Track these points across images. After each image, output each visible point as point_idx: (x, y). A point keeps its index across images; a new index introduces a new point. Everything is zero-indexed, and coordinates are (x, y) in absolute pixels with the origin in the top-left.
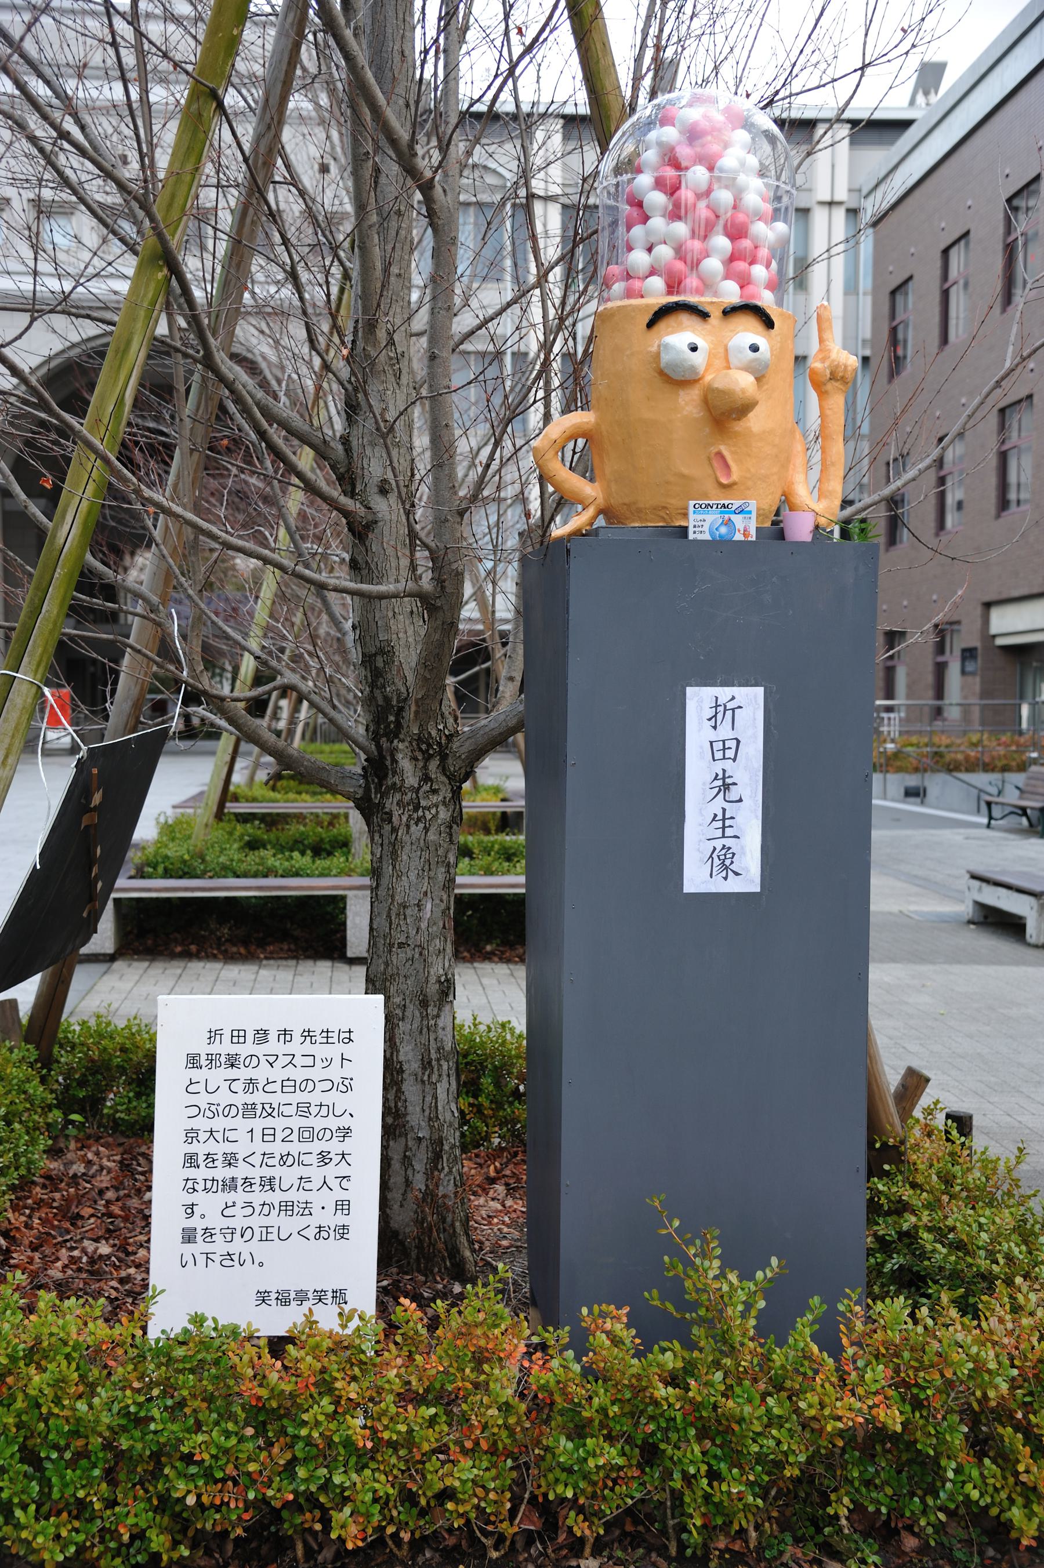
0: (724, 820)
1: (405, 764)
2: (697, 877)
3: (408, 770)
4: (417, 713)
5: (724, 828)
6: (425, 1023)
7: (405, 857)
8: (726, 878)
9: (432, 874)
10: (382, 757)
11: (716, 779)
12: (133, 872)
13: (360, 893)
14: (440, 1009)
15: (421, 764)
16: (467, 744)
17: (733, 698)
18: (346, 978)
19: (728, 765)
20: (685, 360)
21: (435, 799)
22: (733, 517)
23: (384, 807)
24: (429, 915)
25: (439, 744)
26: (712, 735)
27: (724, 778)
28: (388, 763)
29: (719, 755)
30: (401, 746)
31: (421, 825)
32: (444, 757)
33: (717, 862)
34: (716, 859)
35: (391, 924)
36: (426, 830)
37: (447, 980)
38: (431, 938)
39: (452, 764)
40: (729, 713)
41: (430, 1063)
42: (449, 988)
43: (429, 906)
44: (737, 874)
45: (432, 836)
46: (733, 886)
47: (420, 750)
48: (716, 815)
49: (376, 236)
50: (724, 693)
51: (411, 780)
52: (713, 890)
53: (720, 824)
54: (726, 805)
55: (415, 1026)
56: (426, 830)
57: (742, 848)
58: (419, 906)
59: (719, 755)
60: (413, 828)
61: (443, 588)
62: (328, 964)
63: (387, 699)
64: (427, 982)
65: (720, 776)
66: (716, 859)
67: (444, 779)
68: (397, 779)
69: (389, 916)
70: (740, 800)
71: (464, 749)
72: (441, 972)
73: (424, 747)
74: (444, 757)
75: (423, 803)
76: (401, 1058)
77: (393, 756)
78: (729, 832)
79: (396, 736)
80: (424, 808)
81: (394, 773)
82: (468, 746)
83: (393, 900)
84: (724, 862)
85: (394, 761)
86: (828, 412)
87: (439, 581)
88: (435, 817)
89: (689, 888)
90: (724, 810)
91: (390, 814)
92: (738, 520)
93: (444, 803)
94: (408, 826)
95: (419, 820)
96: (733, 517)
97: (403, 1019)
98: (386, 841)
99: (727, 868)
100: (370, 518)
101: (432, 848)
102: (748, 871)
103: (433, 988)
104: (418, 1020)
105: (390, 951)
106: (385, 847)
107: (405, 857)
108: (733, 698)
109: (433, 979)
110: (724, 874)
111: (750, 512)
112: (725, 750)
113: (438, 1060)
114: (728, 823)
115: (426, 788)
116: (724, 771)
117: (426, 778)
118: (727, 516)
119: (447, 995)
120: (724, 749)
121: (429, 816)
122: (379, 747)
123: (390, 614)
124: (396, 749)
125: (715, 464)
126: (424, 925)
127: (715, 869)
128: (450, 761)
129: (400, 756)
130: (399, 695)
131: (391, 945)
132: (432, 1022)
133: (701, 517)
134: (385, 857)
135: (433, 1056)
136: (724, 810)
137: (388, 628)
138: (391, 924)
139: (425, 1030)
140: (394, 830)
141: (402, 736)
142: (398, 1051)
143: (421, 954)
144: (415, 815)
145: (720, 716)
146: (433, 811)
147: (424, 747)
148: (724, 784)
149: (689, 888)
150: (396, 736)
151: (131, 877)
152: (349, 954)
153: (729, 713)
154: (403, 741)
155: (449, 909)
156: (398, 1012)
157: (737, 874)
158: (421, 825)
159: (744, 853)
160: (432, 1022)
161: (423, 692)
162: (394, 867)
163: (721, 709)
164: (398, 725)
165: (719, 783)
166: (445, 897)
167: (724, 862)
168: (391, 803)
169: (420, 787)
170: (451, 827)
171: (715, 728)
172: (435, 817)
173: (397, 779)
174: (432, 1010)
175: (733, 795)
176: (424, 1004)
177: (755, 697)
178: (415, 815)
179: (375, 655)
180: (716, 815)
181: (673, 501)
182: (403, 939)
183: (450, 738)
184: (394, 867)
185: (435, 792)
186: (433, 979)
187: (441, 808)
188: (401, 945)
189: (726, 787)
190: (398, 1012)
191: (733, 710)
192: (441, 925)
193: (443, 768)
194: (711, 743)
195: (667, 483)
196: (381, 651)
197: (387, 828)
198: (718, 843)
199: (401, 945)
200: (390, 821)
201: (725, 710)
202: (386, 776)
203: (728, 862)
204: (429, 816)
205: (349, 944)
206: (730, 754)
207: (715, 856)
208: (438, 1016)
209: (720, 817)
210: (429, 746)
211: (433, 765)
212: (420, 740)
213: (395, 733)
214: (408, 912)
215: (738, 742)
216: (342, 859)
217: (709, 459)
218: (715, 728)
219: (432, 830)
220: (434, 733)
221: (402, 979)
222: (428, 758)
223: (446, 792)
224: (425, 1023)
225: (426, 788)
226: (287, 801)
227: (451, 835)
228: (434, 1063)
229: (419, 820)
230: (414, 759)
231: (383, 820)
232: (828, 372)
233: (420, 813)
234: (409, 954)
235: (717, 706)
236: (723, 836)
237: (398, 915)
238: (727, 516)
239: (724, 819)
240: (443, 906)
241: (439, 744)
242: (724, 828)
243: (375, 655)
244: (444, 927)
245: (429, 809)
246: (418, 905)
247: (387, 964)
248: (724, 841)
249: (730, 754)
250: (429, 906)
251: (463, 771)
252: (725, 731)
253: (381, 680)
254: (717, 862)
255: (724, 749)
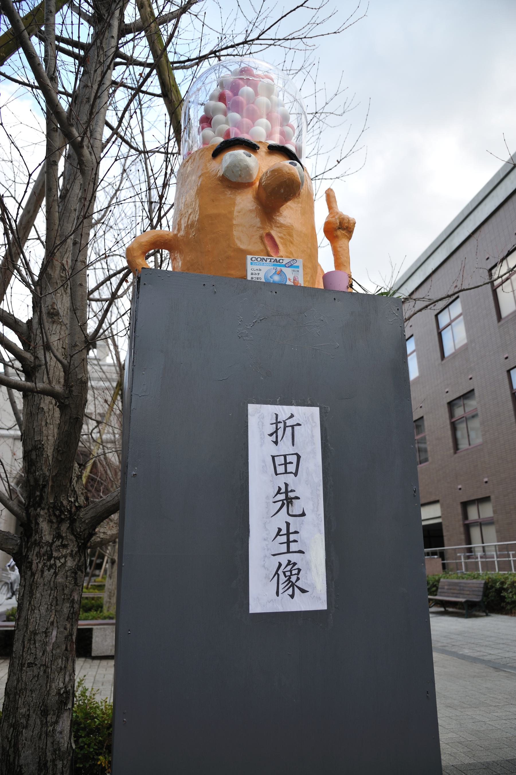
0: (288, 535)
1: (44, 526)
2: (263, 597)
3: (45, 530)
4: (52, 487)
5: (288, 542)
6: (44, 729)
7: (38, 595)
8: (292, 596)
9: (59, 608)
10: (29, 521)
11: (279, 492)
12: (5, 619)
13: (111, 627)
14: (58, 717)
15: (55, 526)
16: (90, 512)
17: (292, 416)
18: (88, 666)
19: (290, 479)
20: (241, 160)
21: (64, 552)
22: (284, 269)
23: (28, 558)
24: (54, 640)
25: (70, 512)
26: (274, 450)
27: (287, 492)
28: (33, 525)
29: (281, 469)
30: (42, 513)
31: (52, 571)
32: (73, 521)
33: (283, 579)
34: (282, 576)
35: (24, 647)
36: (56, 574)
37: (67, 692)
38: (55, 658)
39: (79, 527)
40: (289, 430)
41: (45, 764)
42: (67, 698)
43: (54, 633)
44: (303, 591)
45: (60, 579)
46: (301, 604)
47: (55, 515)
48: (280, 530)
49: (57, 207)
50: (284, 411)
51: (47, 537)
52: (280, 609)
53: (284, 539)
54: (290, 520)
55: (36, 732)
56: (56, 574)
57: (308, 563)
58: (46, 633)
59: (281, 469)
60: (46, 573)
61: (71, 392)
62: (83, 659)
63: (36, 480)
64: (48, 694)
65: (283, 490)
66: (282, 576)
67: (72, 537)
68: (37, 537)
69: (23, 642)
70: (303, 514)
71: (88, 516)
72: (61, 685)
73: (57, 513)
74: (73, 521)
75: (55, 554)
76: (22, 762)
77: (36, 520)
78: (294, 547)
79: (39, 506)
80: (55, 558)
81: (37, 532)
82: (90, 514)
83: (27, 629)
84: (289, 578)
85: (37, 524)
86: (339, 249)
87: (67, 384)
88: (64, 565)
89: (255, 607)
90: (288, 524)
91: (31, 563)
92: (288, 272)
93: (71, 555)
94: (42, 572)
95: (51, 566)
96: (284, 269)
97: (26, 727)
98: (28, 584)
99: (293, 585)
100: (37, 363)
101: (60, 588)
102: (314, 588)
103: (53, 699)
104: (38, 727)
105: (21, 670)
106: (27, 588)
107: (38, 595)
108: (292, 416)
109: (54, 692)
110: (290, 591)
111: (298, 267)
112: (286, 465)
113: (53, 761)
114: (292, 537)
115: (58, 543)
116: (286, 485)
117: (59, 536)
118: (279, 268)
119: (66, 704)
120: (286, 464)
121: (58, 564)
122: (28, 514)
123: (44, 423)
124: (38, 515)
125: (266, 242)
126: (49, 648)
127: (281, 587)
128: (77, 524)
129: (41, 520)
130: (44, 478)
131: (22, 665)
132: (51, 728)
133: (258, 267)
134: (26, 596)
135: (49, 756)
136: (288, 524)
137: (41, 432)
138: (24, 647)
139: (44, 735)
140: (33, 574)
141: (43, 505)
142: (19, 756)
143: (45, 672)
144: (48, 563)
145: (280, 432)
146: (62, 560)
147: (57, 513)
148: (287, 498)
149: (255, 607)
150: (39, 506)
151: (4, 621)
152: (93, 654)
153: (289, 430)
154: (43, 509)
155: (71, 635)
156: (23, 721)
157: (303, 591)
158: (52, 571)
159: (309, 569)
160: (51, 728)
161: (56, 471)
162: (30, 603)
163: (281, 425)
164: (41, 497)
165: (282, 497)
166: (68, 626)
167: (289, 578)
168: (33, 556)
169: (53, 542)
170: (76, 573)
171: (276, 443)
172: (64, 565)
173: (37, 537)
174: (51, 718)
175: (296, 509)
176: (45, 713)
177: (312, 415)
178: (48, 563)
179: (31, 451)
180: (280, 530)
181: (233, 272)
182: (31, 660)
183: (79, 508)
184: (30, 603)
185: (65, 546)
186: (54, 692)
187: (69, 558)
188: (30, 665)
189: (289, 501)
190: (23, 721)
191: (293, 427)
192: (64, 647)
193: (72, 529)
194: (273, 457)
195: (228, 257)
196: (35, 448)
197: (29, 573)
198: (284, 559)
199: (30, 665)
200: (31, 569)
201: (285, 427)
202: (31, 535)
203: (294, 579)
204: (58, 564)
205: (93, 650)
206: (291, 468)
207: (280, 572)
208: (57, 722)
209: (284, 531)
210: (62, 512)
211: (64, 527)
212: (55, 508)
213: (38, 504)
214: (38, 638)
215: (299, 457)
216: (95, 613)
217: (261, 238)
218: (276, 443)
219: (61, 574)
220: (65, 503)
221: (28, 693)
222: (61, 521)
223: (73, 547)
224: (44, 729)
225: (58, 543)
226: (89, 592)
227: (76, 579)
228: (49, 764)
229: (51, 566)
230: (50, 522)
231: (27, 568)
232: (338, 221)
233: (52, 562)
234: (36, 672)
235: (277, 423)
236: (288, 552)
237: (30, 640)
238: (279, 268)
239: (288, 534)
240: (66, 633)
241: (70, 512)
242: (288, 542)
243: (31, 451)
244: (66, 649)
245: (59, 558)
246: (45, 632)
247: (18, 681)
248: (289, 556)
249: (291, 468)
250: (54, 633)
251: (87, 532)
252: (285, 447)
253: (34, 468)
254: (283, 579)
255: (286, 464)
